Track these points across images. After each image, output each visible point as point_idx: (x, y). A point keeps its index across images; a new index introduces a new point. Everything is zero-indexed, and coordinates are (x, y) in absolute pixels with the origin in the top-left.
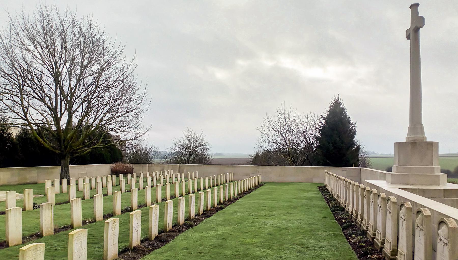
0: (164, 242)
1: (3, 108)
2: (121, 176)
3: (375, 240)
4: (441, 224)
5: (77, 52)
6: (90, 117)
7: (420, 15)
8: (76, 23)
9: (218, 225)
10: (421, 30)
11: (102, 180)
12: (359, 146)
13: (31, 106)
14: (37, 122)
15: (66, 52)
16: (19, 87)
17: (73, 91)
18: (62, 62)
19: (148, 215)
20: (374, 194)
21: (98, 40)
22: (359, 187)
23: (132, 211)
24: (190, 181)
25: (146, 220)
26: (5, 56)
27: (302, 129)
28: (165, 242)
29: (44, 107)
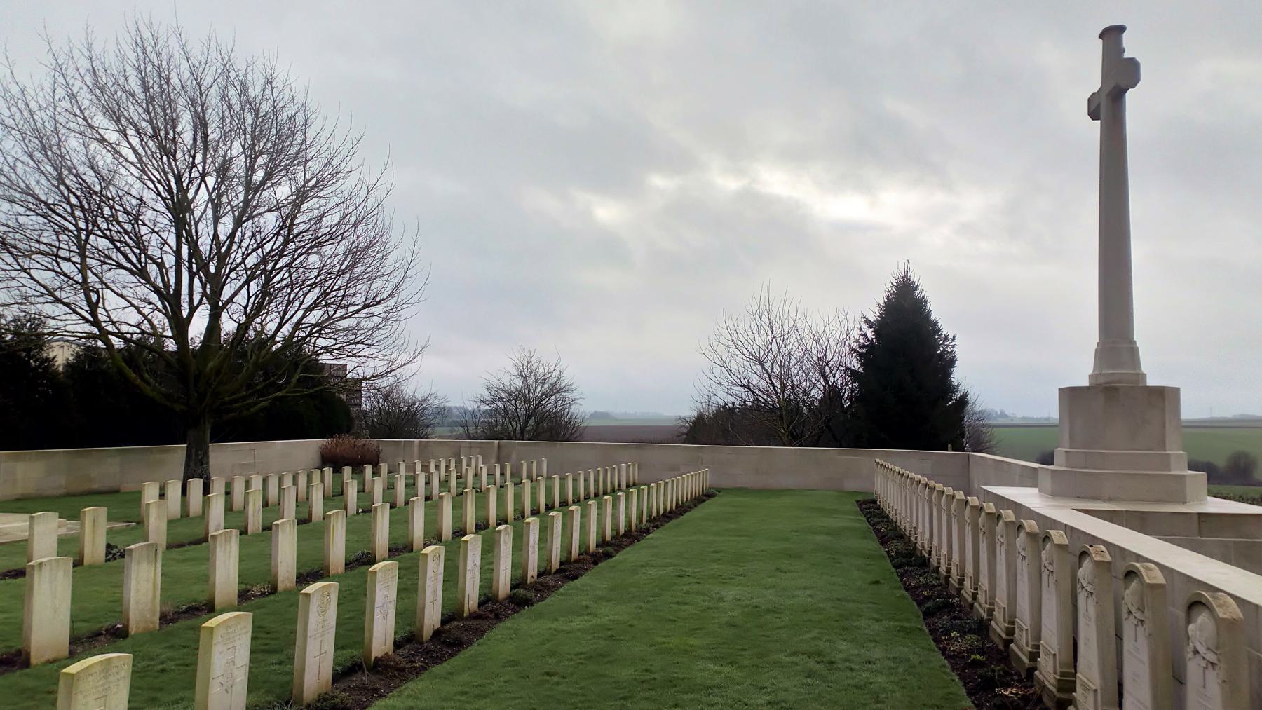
0: (456, 645)
1: (29, 291)
2: (347, 470)
3: (1012, 645)
4: (1196, 610)
5: (237, 148)
6: (268, 319)
7: (1126, 55)
8: (233, 75)
9: (598, 599)
10: (1130, 95)
11: (295, 482)
12: (965, 395)
13: (108, 287)
14: (124, 328)
15: (206, 149)
16: (78, 237)
17: (223, 250)
18: (195, 174)
19: (417, 573)
20: (1007, 524)
21: (292, 118)
22: (967, 502)
23: (374, 562)
24: (528, 485)
25: (409, 588)
26: (37, 155)
27: (815, 352)
28: (457, 645)
29: (144, 291)
